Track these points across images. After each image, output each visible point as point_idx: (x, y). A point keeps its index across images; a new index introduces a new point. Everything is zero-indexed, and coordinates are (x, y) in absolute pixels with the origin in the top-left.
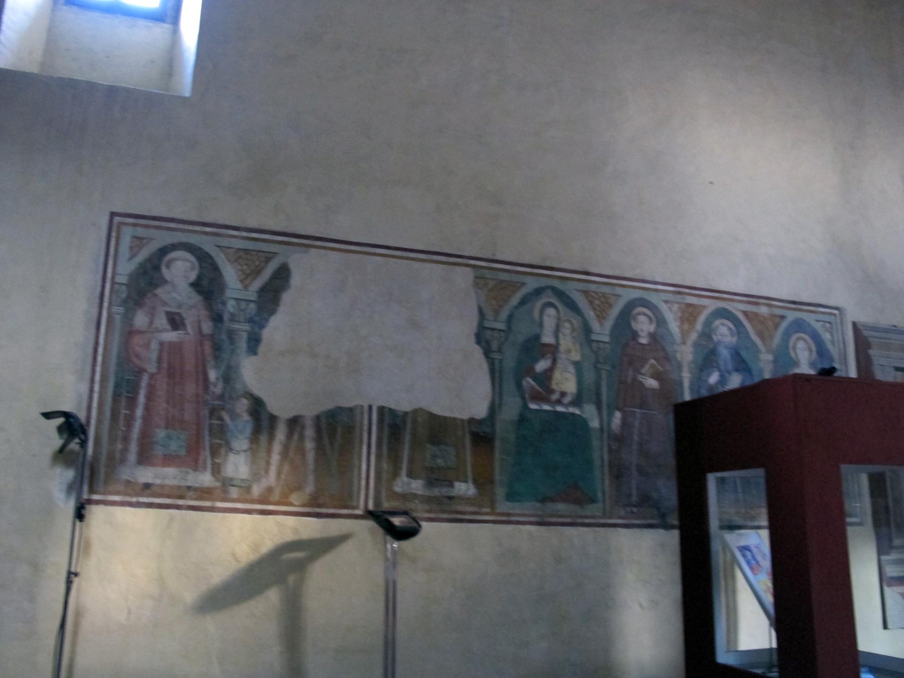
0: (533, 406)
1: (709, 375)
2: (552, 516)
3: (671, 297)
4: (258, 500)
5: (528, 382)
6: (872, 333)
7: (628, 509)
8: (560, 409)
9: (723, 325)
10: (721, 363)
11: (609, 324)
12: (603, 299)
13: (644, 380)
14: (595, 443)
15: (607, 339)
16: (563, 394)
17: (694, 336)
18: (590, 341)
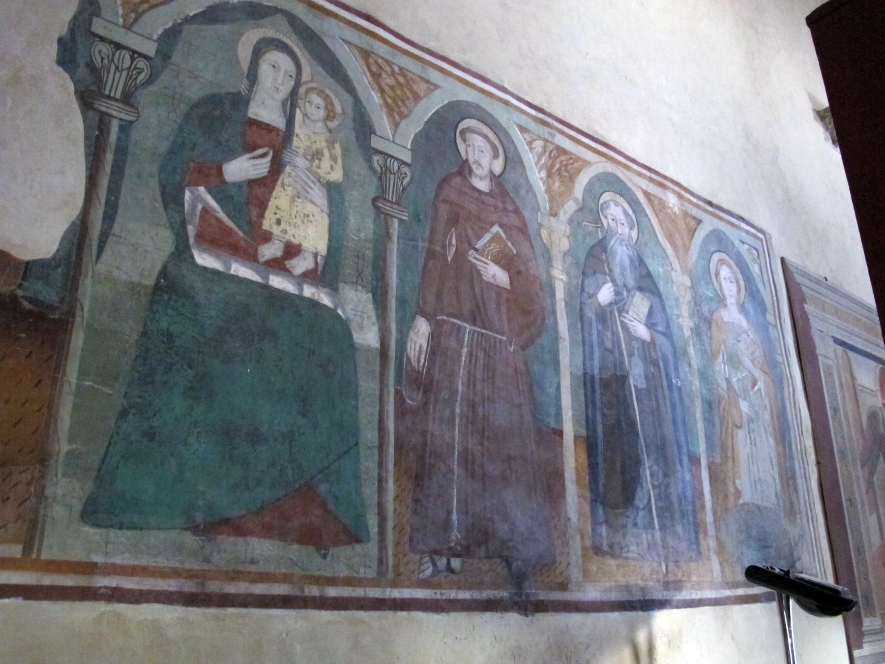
0: (204, 259)
1: (599, 288)
2: (236, 576)
3: (533, 126)
4: (227, 573)
5: (197, 198)
6: (808, 283)
7: (442, 562)
8: (277, 282)
9: (617, 204)
10: (617, 271)
11: (411, 128)
12: (401, 79)
13: (482, 264)
14: (368, 385)
15: (407, 157)
16: (292, 250)
17: (570, 207)
18: (368, 151)
